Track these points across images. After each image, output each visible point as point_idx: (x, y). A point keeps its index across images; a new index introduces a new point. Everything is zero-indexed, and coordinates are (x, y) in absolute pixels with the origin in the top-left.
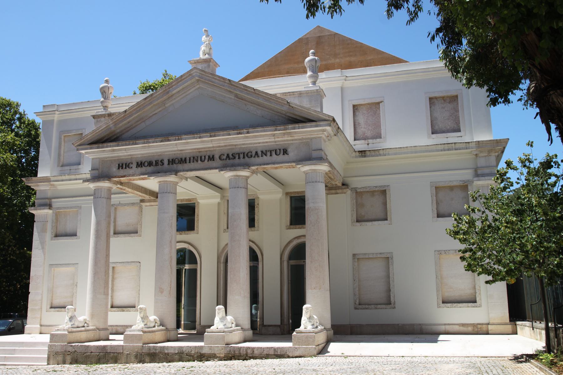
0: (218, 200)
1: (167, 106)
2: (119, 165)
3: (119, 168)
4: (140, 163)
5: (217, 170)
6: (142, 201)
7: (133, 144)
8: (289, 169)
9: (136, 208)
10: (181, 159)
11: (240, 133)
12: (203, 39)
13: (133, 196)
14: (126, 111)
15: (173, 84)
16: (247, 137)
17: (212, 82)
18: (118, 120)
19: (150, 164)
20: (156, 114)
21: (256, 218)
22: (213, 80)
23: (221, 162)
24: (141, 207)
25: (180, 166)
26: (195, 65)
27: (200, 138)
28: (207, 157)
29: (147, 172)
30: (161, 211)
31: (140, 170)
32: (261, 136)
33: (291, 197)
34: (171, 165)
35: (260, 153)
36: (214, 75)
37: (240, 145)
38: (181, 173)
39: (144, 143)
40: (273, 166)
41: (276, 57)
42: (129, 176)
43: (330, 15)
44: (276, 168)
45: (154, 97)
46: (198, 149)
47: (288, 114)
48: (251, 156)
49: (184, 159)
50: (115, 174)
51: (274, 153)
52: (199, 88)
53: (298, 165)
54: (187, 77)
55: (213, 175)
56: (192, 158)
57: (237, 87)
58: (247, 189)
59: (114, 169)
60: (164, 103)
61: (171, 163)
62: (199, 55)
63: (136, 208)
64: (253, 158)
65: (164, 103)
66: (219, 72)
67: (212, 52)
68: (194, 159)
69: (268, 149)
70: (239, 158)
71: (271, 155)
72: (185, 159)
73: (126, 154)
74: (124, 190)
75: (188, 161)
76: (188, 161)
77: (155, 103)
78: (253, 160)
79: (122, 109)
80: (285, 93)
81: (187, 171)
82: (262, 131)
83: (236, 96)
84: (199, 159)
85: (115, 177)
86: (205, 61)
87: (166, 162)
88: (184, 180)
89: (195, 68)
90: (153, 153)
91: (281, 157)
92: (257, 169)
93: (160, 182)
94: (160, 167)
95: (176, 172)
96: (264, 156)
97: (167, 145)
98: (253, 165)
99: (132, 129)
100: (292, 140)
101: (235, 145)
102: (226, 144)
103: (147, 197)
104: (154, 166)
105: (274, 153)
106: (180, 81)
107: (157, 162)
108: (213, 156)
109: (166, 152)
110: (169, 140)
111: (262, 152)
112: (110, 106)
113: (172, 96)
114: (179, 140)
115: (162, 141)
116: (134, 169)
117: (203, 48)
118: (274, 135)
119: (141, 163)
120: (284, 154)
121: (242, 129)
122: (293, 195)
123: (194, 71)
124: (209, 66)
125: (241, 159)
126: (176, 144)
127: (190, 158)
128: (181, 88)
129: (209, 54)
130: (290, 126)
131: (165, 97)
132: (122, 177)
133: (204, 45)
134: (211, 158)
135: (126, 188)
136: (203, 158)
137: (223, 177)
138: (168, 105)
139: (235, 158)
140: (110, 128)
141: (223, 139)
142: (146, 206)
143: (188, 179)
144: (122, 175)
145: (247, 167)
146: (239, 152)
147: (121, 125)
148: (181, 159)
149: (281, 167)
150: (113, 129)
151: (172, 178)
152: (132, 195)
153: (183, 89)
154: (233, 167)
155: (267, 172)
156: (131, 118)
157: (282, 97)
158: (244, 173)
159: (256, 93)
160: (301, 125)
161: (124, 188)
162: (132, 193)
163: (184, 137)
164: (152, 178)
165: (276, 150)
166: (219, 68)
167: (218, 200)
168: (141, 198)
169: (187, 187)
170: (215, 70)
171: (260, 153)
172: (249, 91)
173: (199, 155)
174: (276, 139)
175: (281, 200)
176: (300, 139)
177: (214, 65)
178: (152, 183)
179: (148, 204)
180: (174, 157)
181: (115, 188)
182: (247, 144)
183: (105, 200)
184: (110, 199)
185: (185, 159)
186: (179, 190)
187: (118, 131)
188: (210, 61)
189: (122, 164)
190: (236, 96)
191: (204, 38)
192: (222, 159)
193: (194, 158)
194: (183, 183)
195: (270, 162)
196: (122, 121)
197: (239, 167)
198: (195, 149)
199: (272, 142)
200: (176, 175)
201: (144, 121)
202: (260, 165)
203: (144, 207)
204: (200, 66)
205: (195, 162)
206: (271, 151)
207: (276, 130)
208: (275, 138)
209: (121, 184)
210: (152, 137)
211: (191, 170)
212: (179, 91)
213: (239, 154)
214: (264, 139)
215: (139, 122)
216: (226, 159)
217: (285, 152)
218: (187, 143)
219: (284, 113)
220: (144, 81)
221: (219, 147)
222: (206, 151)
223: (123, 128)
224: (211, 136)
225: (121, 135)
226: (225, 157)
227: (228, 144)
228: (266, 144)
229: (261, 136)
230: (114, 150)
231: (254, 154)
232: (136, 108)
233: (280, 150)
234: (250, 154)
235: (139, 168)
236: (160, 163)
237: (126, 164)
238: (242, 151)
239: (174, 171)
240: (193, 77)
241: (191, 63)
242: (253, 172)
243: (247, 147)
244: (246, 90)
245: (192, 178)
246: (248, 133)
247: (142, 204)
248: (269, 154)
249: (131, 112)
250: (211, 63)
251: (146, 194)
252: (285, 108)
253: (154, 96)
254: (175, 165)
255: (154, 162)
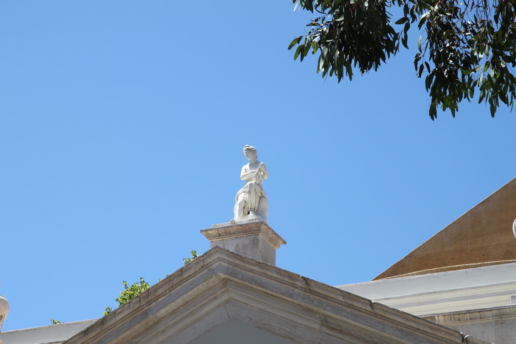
12: (243, 173)
15: (160, 292)
17: (259, 285)
22: (264, 279)
26: (218, 242)
36: (266, 265)
41: (473, 214)
43: (486, 105)
45: (109, 328)
52: (227, 302)
54: (195, 273)
57: (326, 297)
62: (233, 215)
66: (285, 260)
67: (268, 205)
80: (459, 313)
83: (325, 322)
86: (246, 230)
89: (216, 249)
106: (178, 284)
113: (156, 323)
117: (242, 196)
123: (216, 256)
124: (255, 243)
128: (180, 301)
129: (257, 212)
131: (137, 328)
133: (246, 188)
153: (186, 304)
157: (450, 324)
159: (376, 315)
166: (282, 246)
170: (274, 252)
172: (359, 310)
177: (270, 240)
188: (259, 230)
190: (325, 322)
191: (246, 170)
204: (231, 245)
212: (174, 312)
220: (133, 281)
240: (213, 272)
241: (209, 237)
244: (351, 306)
250: (261, 236)
253: (109, 324)
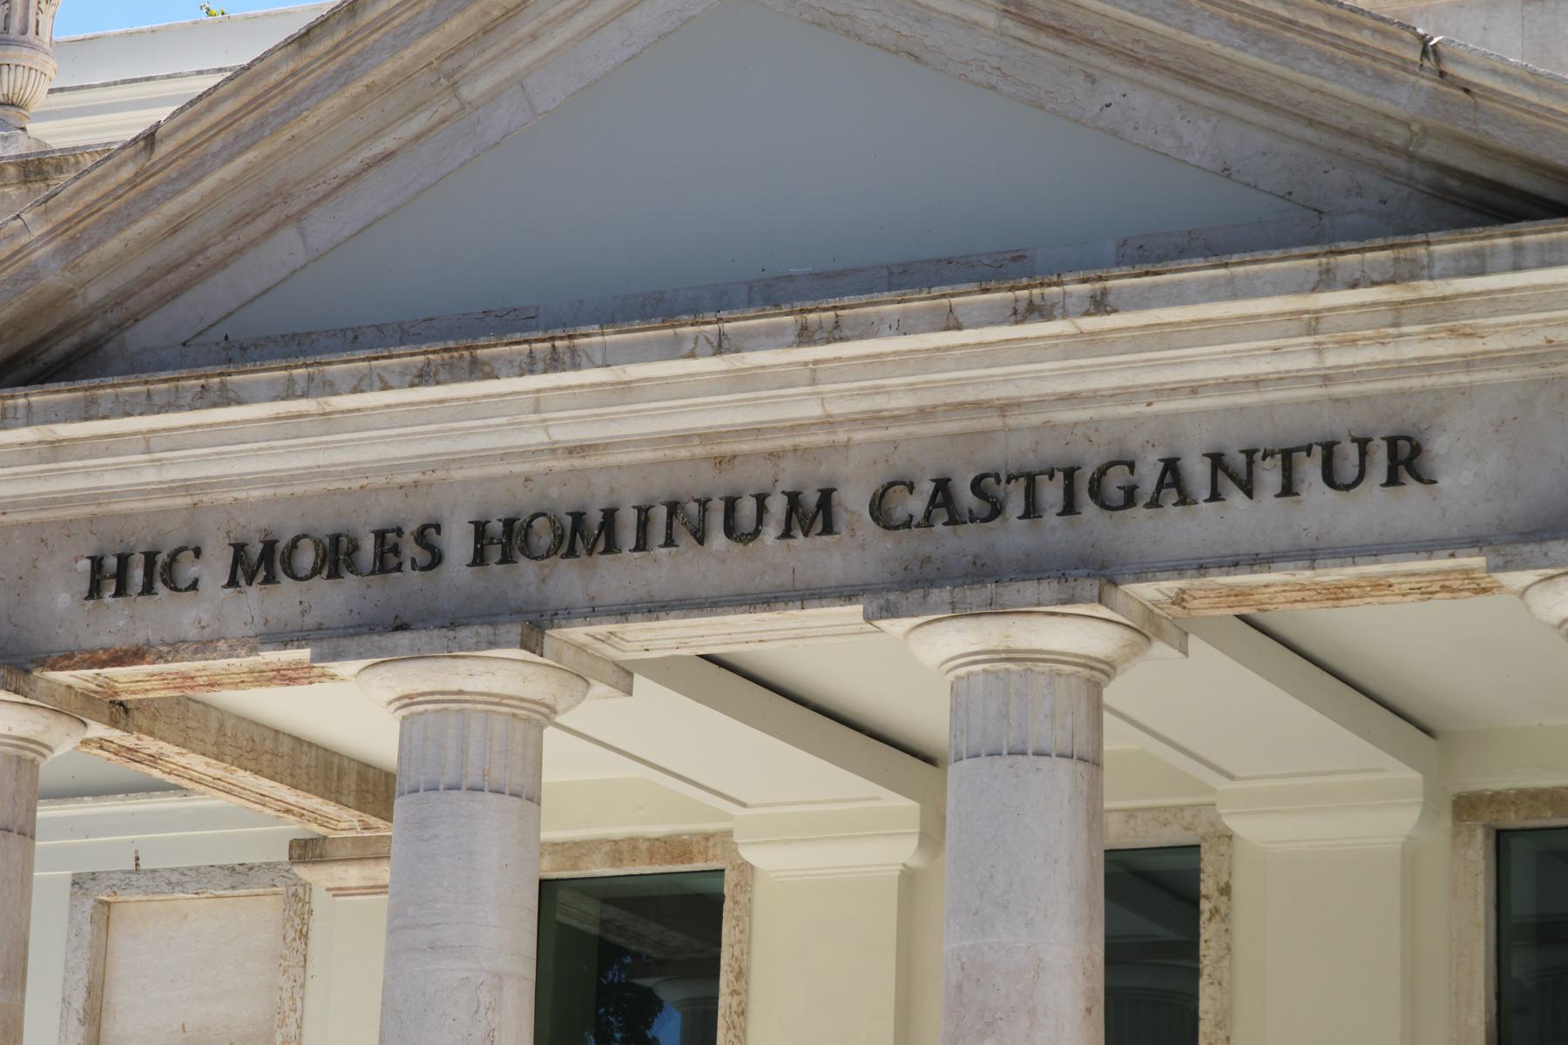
0: (904, 851)
1: (466, 92)
2: (97, 563)
3: (95, 591)
4: (256, 549)
5: (856, 610)
6: (307, 851)
7: (205, 399)
8: (1441, 603)
9: (259, 913)
10: (578, 518)
11: (1035, 311)
13: (246, 817)
14: (150, 139)
16: (1094, 342)
18: (91, 209)
19: (336, 556)
20: (388, 156)
21: (1205, 1004)
23: (886, 545)
24: (299, 900)
25: (568, 578)
27: (721, 346)
28: (777, 505)
29: (310, 621)
30: (412, 936)
31: (255, 601)
32: (1207, 331)
33: (1502, 840)
34: (495, 568)
35: (1197, 472)
37: (1040, 403)
38: (578, 633)
39: (289, 393)
40: (1305, 576)
42: (174, 648)
44: (1337, 594)
45: (372, 27)
46: (705, 437)
47: (1433, 150)
48: (1130, 497)
49: (595, 518)
50: (64, 639)
51: (1310, 469)
53: (1506, 566)
55: (824, 644)
56: (660, 513)
58: (1094, 762)
59: (60, 595)
60: (446, 72)
61: (495, 552)
63: (259, 913)
64: (1139, 512)
65: (446, 72)
68: (679, 519)
69: (1264, 436)
70: (1032, 510)
71: (1288, 489)
72: (610, 515)
73: (150, 476)
74: (154, 760)
75: (628, 536)
76: (628, 536)
77: (377, 75)
78: (1142, 528)
79: (126, 126)
81: (624, 612)
82: (1210, 293)
84: (717, 520)
85: (67, 660)
87: (458, 544)
88: (599, 688)
90: (359, 470)
91: (1374, 507)
92: (1179, 600)
93: (409, 700)
94: (410, 580)
95: (534, 625)
96: (1236, 498)
97: (470, 406)
98: (1145, 572)
99: (202, 276)
100: (1468, 363)
101: (1004, 408)
102: (927, 399)
103: (345, 821)
104: (371, 572)
105: (1310, 469)
107: (387, 544)
108: (826, 495)
109: (461, 460)
110: (478, 370)
111: (1217, 461)
112: (40, 101)
114: (554, 363)
115: (423, 377)
116: (213, 599)
118: (1312, 323)
119: (509, 523)
120: (1393, 480)
121: (1056, 272)
122: (1512, 820)
125: (1051, 518)
126: (537, 402)
127: (644, 514)
130: (1446, 248)
132: (119, 658)
134: (813, 513)
135: (169, 749)
136: (747, 508)
137: (909, 664)
138: (484, 84)
139: (996, 510)
140: (34, 274)
141: (901, 361)
142: (339, 892)
143: (639, 680)
144: (120, 643)
145: (1090, 587)
146: (1031, 462)
147: (113, 246)
148: (578, 518)
149: (1379, 586)
150: (55, 278)
151: (498, 672)
152: (221, 801)
154: (977, 583)
155: (1264, 618)
156: (194, 194)
158: (1072, 633)
160: (1534, 236)
161: (151, 745)
162: (218, 785)
163: (596, 340)
164: (347, 668)
165: (1329, 449)
167: (904, 851)
168: (296, 828)
169: (627, 749)
171: (1197, 472)
173: (717, 485)
174: (1334, 359)
175: (1411, 855)
176: (1530, 357)
178: (355, 705)
179: (352, 875)
180: (523, 502)
181: (66, 746)
182: (1095, 397)
183: (1064, 775)
184: (27, 833)
185: (610, 515)
186: (563, 762)
187: (95, 293)
189: (123, 560)
192: (899, 514)
193: (673, 508)
194: (598, 709)
195: (1282, 542)
196: (124, 218)
197: (1030, 589)
198: (684, 438)
199: (1300, 378)
200: (532, 640)
201: (297, 218)
202: (1202, 568)
203: (320, 900)
205: (685, 539)
206: (1287, 455)
207: (1327, 280)
208: (1319, 349)
209: (120, 711)
210: (352, 339)
211: (654, 608)
213: (1031, 480)
214: (1237, 357)
215: (262, 224)
216: (928, 521)
217: (1406, 460)
218: (624, 390)
219: (1399, 136)
221: (875, 419)
222: (773, 455)
223: (135, 270)
224: (805, 336)
225: (120, 327)
226: (916, 505)
227: (970, 395)
228: (1251, 398)
229: (1207, 331)
230: (56, 448)
231: (1148, 475)
232: (234, 117)
233: (1363, 444)
234: (1116, 480)
235: (253, 592)
236: (410, 549)
237: (150, 558)
238: (1053, 452)
239: (517, 612)
242: (1146, 628)
243: (1095, 425)
245: (667, 671)
246: (1100, 304)
247: (303, 872)
248: (1269, 475)
249: (187, 148)
251: (333, 793)
252: (1407, 99)
254: (526, 568)
255: (368, 545)
